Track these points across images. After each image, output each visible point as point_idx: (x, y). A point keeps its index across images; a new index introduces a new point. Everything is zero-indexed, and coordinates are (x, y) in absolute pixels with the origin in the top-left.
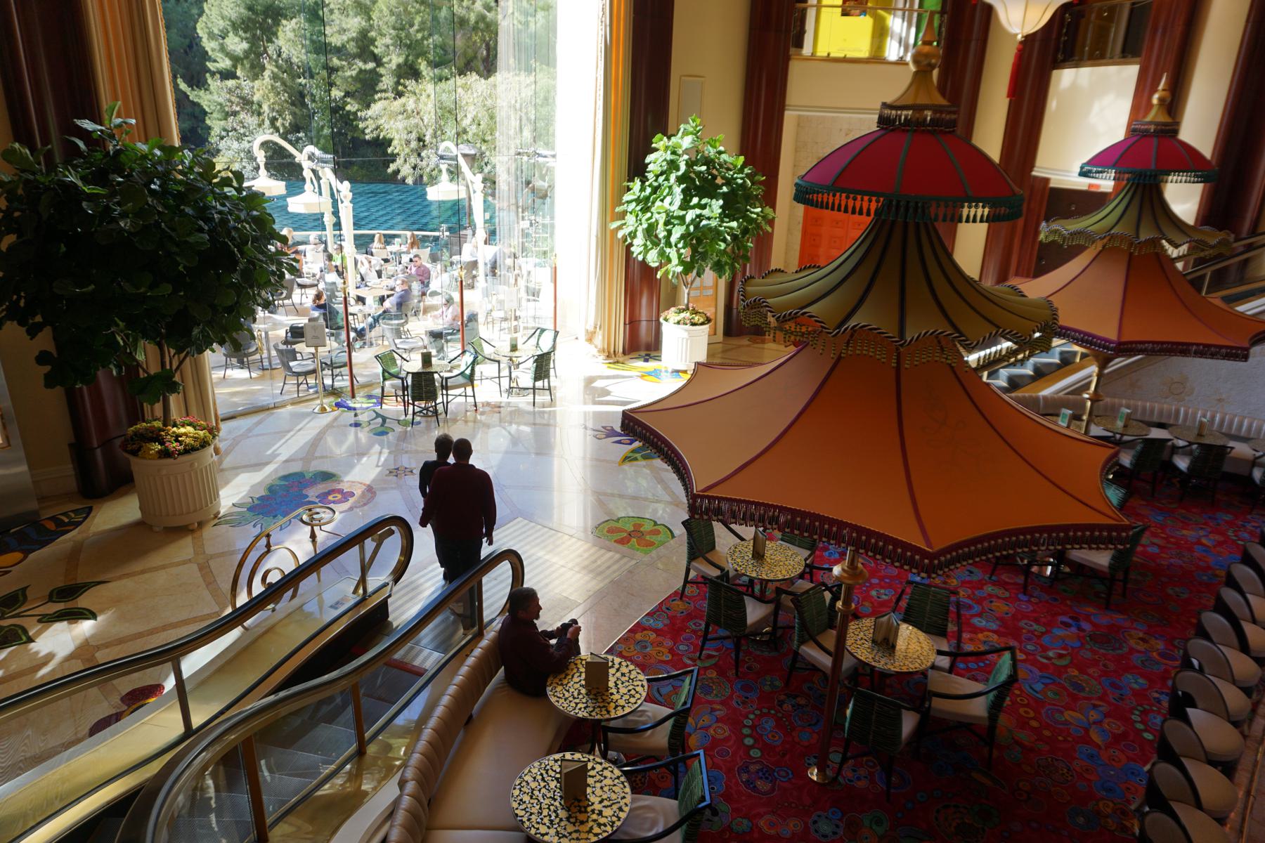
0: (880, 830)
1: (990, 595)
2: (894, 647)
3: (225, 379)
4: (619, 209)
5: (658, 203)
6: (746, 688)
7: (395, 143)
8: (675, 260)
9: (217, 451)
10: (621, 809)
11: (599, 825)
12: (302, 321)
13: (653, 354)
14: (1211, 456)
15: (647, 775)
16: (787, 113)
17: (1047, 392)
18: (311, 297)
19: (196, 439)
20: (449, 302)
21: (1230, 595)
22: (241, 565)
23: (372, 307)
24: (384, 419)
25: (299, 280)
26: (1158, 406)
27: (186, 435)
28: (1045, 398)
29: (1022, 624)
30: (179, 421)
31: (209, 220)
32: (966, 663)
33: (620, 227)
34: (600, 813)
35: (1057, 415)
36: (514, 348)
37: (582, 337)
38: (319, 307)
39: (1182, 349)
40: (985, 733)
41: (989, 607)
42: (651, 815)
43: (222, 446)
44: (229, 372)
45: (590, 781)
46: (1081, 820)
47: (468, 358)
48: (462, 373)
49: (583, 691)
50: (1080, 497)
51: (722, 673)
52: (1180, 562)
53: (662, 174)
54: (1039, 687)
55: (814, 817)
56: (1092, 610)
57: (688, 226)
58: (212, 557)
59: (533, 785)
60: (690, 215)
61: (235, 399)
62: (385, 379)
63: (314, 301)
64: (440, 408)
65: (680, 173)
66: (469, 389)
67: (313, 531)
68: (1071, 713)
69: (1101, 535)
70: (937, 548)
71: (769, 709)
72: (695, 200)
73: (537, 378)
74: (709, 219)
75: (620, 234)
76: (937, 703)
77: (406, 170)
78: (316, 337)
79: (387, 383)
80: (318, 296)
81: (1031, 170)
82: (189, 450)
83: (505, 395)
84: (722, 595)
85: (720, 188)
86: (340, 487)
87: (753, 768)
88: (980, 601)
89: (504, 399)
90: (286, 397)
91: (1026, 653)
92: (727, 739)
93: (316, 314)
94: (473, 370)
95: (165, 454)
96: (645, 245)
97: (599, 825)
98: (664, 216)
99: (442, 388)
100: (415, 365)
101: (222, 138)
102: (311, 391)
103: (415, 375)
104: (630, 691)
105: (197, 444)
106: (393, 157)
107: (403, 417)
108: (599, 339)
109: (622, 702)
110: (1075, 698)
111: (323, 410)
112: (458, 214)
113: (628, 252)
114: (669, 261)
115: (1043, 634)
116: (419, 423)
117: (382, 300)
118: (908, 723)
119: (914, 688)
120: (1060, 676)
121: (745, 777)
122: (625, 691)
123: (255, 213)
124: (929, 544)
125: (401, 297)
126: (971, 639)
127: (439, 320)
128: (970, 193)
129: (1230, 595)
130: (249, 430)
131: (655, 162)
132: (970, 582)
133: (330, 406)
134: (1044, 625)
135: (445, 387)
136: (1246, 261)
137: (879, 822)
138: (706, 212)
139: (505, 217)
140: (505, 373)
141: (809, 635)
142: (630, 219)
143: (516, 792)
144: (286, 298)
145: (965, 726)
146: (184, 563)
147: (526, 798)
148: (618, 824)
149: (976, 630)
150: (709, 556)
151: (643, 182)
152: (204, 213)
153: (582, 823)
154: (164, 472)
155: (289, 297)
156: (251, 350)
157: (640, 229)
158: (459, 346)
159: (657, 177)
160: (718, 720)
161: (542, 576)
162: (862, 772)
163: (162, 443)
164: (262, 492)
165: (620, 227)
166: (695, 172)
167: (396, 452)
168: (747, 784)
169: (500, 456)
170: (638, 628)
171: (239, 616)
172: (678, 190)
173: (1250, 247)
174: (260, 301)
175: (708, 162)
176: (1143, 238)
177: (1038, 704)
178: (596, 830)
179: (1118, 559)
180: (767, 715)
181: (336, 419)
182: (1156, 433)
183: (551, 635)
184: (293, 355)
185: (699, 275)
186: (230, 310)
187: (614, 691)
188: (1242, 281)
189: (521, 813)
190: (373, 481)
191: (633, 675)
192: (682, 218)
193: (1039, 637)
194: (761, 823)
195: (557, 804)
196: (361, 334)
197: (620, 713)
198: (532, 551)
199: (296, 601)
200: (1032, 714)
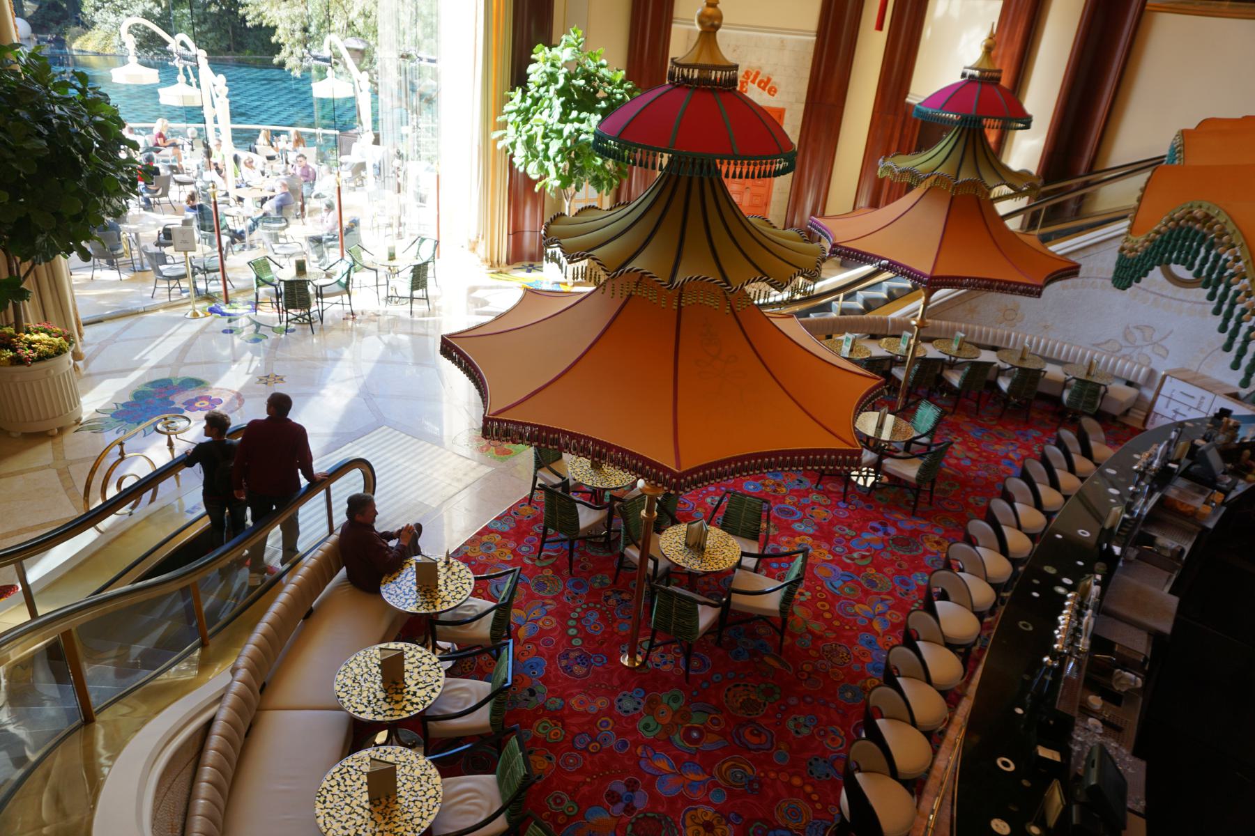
0: (675, 706)
1: (813, 503)
2: (703, 549)
3: (86, 282)
4: (500, 119)
5: (537, 116)
6: (578, 585)
7: (279, 31)
8: (553, 173)
9: (77, 356)
10: (433, 690)
11: (412, 704)
12: (175, 221)
13: (537, 264)
14: (1028, 378)
15: (465, 662)
16: (675, 27)
17: (896, 315)
18: (184, 197)
19: (50, 346)
20: (330, 207)
21: (999, 506)
22: (93, 472)
23: (251, 209)
24: (258, 325)
25: (177, 177)
26: (990, 329)
27: (40, 342)
28: (893, 321)
29: (836, 529)
30: (32, 326)
31: (47, 123)
32: (779, 563)
33: (501, 138)
34: (414, 694)
35: (899, 337)
36: (392, 257)
37: (467, 247)
38: (193, 208)
39: (990, 285)
40: (780, 622)
41: (806, 516)
42: (466, 695)
43: (85, 351)
44: (98, 273)
45: (407, 666)
46: (849, 695)
47: (344, 267)
48: (338, 281)
49: (415, 588)
50: (829, 426)
51: (557, 570)
52: (986, 474)
53: (543, 85)
54: (838, 584)
55: (620, 696)
56: (899, 516)
57: (565, 141)
58: (72, 462)
59: (357, 671)
60: (568, 129)
61: (103, 302)
62: (258, 286)
63: (188, 202)
64: (314, 314)
65: (559, 86)
66: (346, 296)
67: (170, 440)
68: (861, 606)
69: (837, 458)
70: (684, 469)
71: (595, 603)
72: (574, 114)
73: (414, 287)
74: (587, 133)
75: (500, 145)
76: (736, 598)
77: (291, 63)
78: (185, 242)
79: (261, 290)
80: (192, 197)
81: (906, 96)
82: (43, 357)
83: (383, 303)
84: (557, 502)
85: (599, 102)
86: (207, 394)
87: (573, 655)
88: (802, 509)
89: (382, 307)
90: (158, 301)
91: (834, 555)
92: (555, 629)
93: (191, 215)
94: (348, 278)
95: (18, 361)
96: (526, 157)
97: (412, 704)
98: (542, 128)
99: (317, 296)
100: (290, 273)
101: (97, 9)
102: (185, 295)
103: (288, 284)
104: (457, 590)
105: (52, 352)
106: (278, 48)
107: (277, 324)
108: (482, 250)
109: (448, 598)
110: (866, 593)
111: (196, 315)
112: (341, 118)
113: (511, 164)
114: (547, 174)
115: (853, 537)
116: (293, 330)
117: (263, 201)
118: (706, 617)
119: (718, 585)
120: (858, 575)
121: (564, 662)
122: (452, 588)
123: (99, 119)
124: (678, 466)
125: (281, 200)
126: (788, 542)
127: (320, 224)
128: (736, 151)
129: (999, 506)
130: (117, 335)
131: (536, 72)
132: (797, 491)
133: (203, 311)
134: (856, 529)
135: (320, 295)
136: (1082, 197)
137: (676, 699)
138: (584, 127)
139: (387, 119)
140: (383, 281)
141: (631, 541)
142: (511, 129)
143: (341, 677)
144: (161, 196)
145: (763, 618)
146: (43, 468)
147: (349, 682)
148: (430, 702)
149: (794, 534)
150: (553, 466)
151: (525, 92)
152: (42, 117)
153: (397, 702)
154: (18, 379)
155: (165, 194)
156: (120, 251)
157: (519, 140)
158: (338, 251)
159: (539, 87)
160: (548, 613)
161: (393, 486)
162: (669, 657)
163: (14, 350)
164: (127, 398)
165: (501, 138)
166: (574, 86)
167: (270, 359)
168: (565, 668)
169: (372, 365)
170: (487, 530)
171: (89, 519)
172: (557, 102)
173: (1087, 185)
174: (109, 209)
175: (589, 77)
176: (962, 178)
177: (834, 598)
178: (409, 708)
179: (924, 471)
180: (593, 609)
181: (208, 325)
182: (986, 356)
183: (389, 536)
184: (162, 258)
185: (577, 189)
186: (76, 218)
187: (443, 588)
188: (1078, 214)
189: (341, 694)
190: (242, 389)
191: (463, 572)
192: (560, 132)
193: (848, 541)
194: (573, 702)
195: (376, 686)
196: (237, 236)
197: (445, 607)
198: (400, 462)
199: (155, 506)
200: (827, 607)
